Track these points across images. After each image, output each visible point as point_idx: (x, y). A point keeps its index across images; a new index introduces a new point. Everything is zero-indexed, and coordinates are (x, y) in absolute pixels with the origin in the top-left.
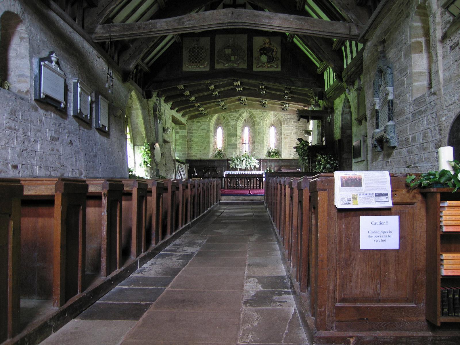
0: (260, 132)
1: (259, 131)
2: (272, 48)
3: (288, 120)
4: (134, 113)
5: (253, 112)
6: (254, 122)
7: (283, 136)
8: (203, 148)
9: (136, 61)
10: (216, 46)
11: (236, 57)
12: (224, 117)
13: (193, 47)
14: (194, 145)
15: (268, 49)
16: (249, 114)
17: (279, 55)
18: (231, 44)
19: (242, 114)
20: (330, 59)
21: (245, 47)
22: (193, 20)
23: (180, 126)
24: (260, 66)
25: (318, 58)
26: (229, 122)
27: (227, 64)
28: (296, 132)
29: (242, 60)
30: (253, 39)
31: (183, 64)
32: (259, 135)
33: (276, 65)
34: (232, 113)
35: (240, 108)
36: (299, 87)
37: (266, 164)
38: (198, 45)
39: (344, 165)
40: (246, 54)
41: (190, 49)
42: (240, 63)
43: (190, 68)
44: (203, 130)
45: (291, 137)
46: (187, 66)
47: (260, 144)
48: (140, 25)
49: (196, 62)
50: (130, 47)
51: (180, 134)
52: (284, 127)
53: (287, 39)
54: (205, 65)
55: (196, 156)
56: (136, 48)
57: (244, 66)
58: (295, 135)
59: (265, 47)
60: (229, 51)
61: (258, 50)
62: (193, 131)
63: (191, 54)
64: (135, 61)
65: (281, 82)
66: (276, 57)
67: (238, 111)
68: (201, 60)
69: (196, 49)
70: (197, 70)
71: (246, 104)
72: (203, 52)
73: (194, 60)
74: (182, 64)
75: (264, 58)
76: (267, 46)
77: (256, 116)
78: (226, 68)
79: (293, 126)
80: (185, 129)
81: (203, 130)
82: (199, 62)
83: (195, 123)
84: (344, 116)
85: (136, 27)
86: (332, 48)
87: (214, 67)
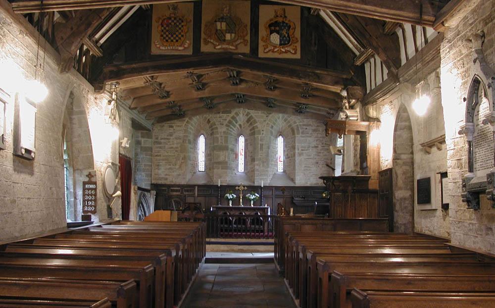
0: (263, 145)
1: (261, 143)
2: (287, 24)
4: (74, 118)
6: (253, 128)
11: (233, 35)
13: (168, 18)
15: (281, 24)
16: (246, 117)
17: (298, 34)
19: (235, 116)
21: (247, 20)
23: (142, 133)
24: (269, 51)
25: (358, 42)
26: (217, 128)
27: (219, 45)
28: (316, 145)
29: (242, 41)
32: (261, 148)
33: (293, 49)
34: (221, 115)
35: (234, 108)
36: (327, 84)
37: (271, 192)
38: (175, 14)
41: (163, 21)
43: (162, 50)
46: (158, 46)
47: (263, 162)
49: (172, 41)
52: (298, 137)
54: (186, 46)
55: (166, 179)
58: (315, 149)
59: (276, 22)
61: (267, 26)
62: (162, 141)
63: (165, 28)
67: (230, 113)
69: (173, 21)
72: (182, 26)
73: (170, 38)
75: (275, 38)
76: (280, 20)
79: (310, 137)
80: (149, 137)
81: (176, 138)
83: (165, 128)
84: (398, 133)
86: (384, 30)
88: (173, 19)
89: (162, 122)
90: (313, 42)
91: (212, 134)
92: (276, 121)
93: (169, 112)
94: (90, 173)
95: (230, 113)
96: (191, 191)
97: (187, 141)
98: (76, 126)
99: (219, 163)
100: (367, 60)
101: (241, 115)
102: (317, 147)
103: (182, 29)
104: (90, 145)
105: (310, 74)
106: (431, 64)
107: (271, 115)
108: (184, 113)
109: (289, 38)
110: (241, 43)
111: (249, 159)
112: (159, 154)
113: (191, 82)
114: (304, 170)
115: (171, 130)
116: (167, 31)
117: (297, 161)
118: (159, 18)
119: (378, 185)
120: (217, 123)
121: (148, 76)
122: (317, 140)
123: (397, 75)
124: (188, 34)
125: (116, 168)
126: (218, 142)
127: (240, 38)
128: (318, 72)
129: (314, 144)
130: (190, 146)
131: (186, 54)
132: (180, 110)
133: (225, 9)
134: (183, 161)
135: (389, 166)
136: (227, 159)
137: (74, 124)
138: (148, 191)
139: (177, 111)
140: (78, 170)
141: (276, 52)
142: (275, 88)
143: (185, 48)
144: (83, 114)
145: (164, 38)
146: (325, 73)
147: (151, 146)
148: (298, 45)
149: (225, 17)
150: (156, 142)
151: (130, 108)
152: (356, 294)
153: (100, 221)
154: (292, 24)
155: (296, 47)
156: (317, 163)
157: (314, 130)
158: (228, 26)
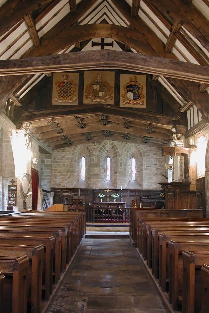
2: (137, 86)
5: (115, 144)
6: (116, 153)
7: (143, 167)
10: (85, 82)
11: (104, 93)
12: (88, 147)
17: (144, 92)
19: (104, 145)
21: (112, 83)
22: (70, 59)
24: (127, 103)
26: (93, 153)
27: (95, 99)
30: (120, 76)
31: (53, 97)
32: (121, 165)
34: (96, 144)
35: (103, 140)
38: (67, 80)
41: (59, 84)
43: (59, 102)
45: (150, 168)
46: (56, 100)
48: (16, 62)
49: (65, 97)
53: (152, 78)
54: (74, 100)
55: (60, 185)
58: (155, 166)
59: (131, 85)
62: (58, 160)
63: (61, 89)
65: (146, 118)
66: (142, 95)
69: (66, 84)
71: (109, 136)
72: (72, 87)
73: (64, 95)
76: (133, 83)
77: (118, 147)
80: (50, 158)
81: (67, 159)
82: (68, 97)
83: (59, 152)
85: (12, 64)
88: (66, 83)
90: (154, 97)
92: (130, 148)
93: (62, 142)
96: (76, 192)
99: (94, 175)
100: (188, 109)
101: (108, 144)
102: (157, 164)
103: (72, 89)
105: (152, 117)
111: (113, 172)
115: (64, 154)
116: (62, 90)
117: (144, 174)
118: (57, 82)
119: (196, 188)
121: (49, 119)
124: (75, 93)
126: (93, 161)
131: (74, 105)
132: (70, 141)
133: (99, 77)
134: (71, 173)
136: (99, 172)
140: (5, 177)
142: (130, 126)
143: (74, 101)
145: (60, 95)
147: (51, 164)
148: (145, 100)
149: (98, 82)
153: (19, 211)
154: (141, 86)
156: (157, 175)
157: (154, 154)
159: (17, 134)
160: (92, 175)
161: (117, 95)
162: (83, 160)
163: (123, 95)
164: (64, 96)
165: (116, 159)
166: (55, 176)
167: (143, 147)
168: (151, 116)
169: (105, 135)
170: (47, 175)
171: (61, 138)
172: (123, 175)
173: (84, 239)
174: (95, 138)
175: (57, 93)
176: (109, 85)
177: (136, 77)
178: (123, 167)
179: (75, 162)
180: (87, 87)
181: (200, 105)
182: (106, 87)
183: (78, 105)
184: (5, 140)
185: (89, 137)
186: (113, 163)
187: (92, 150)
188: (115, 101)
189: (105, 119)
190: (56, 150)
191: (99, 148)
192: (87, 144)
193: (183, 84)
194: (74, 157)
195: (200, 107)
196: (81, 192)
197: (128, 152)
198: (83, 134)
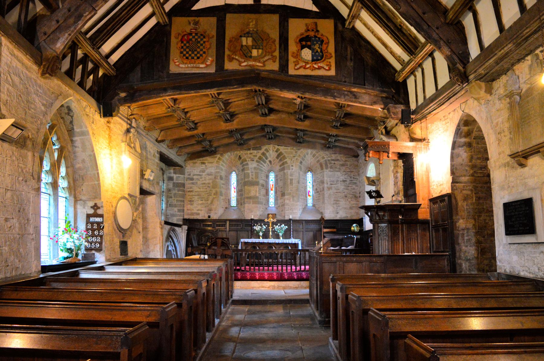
2: (319, 38)
3: (333, 162)
5: (281, 150)
7: (326, 185)
8: (209, 202)
9: (70, 35)
11: (260, 51)
14: (196, 197)
17: (331, 48)
18: (251, 29)
19: (265, 152)
20: (441, 39)
21: (275, 35)
23: (174, 169)
24: (301, 67)
26: (247, 164)
27: (244, 62)
29: (270, 57)
30: (288, 22)
32: (291, 183)
33: (327, 65)
34: (252, 151)
35: (264, 144)
36: (365, 103)
37: (301, 225)
38: (196, 30)
39: (460, 241)
40: (278, 46)
42: (266, 61)
43: (182, 68)
44: (208, 175)
46: (177, 64)
47: (293, 197)
49: (193, 58)
50: (59, 8)
51: (175, 181)
54: (208, 63)
55: (198, 214)
56: (69, 11)
57: (275, 66)
59: (308, 36)
60: (248, 42)
61: (298, 41)
62: (195, 177)
63: (185, 45)
64: (67, 35)
67: (260, 148)
68: (201, 55)
70: (193, 72)
71: (272, 138)
72: (204, 42)
73: (190, 55)
74: (169, 62)
75: (307, 54)
76: (312, 34)
77: (286, 155)
78: (243, 68)
80: (183, 173)
81: (208, 175)
82: (198, 58)
83: (197, 164)
84: (456, 151)
86: (446, 18)
87: (223, 67)
88: (194, 35)
89: (195, 159)
90: (349, 57)
91: (243, 170)
92: (305, 156)
93: (198, 148)
94: (96, 204)
95: (260, 149)
96: (222, 225)
97: (219, 177)
98: (79, 150)
99: (250, 198)
100: (412, 72)
101: (271, 150)
102: (345, 181)
103: (204, 45)
104: (96, 172)
105: (346, 93)
106: (531, 40)
107: (300, 151)
108: (215, 150)
109: (322, 53)
110: (268, 59)
111: (279, 194)
112: (191, 190)
113: (218, 111)
114: (334, 204)
115: (203, 166)
116: (187, 47)
117: (326, 195)
118: (179, 34)
119: (429, 214)
120: (247, 159)
121: (167, 98)
122: (346, 174)
123: (465, 72)
124: (210, 51)
125: (135, 201)
126: (249, 177)
127: (267, 54)
128: (355, 90)
129: (342, 178)
130: (222, 182)
131: (208, 72)
132: (211, 146)
133: (251, 24)
134: (214, 196)
135: (446, 189)
136: (258, 195)
137: (76, 147)
138: (179, 226)
139: (208, 146)
140: (81, 200)
141: (308, 68)
142: (306, 117)
143: (207, 66)
144: (86, 135)
145: (184, 55)
146: (363, 91)
147: (183, 182)
148: (333, 61)
149: (251, 32)
150: (189, 178)
151: (157, 140)
152: (372, 314)
153: (107, 260)
154: (325, 39)
155: (330, 62)
156: (346, 197)
157: (343, 165)
158: (254, 42)
159: (109, 125)
160: (248, 198)
161: (283, 54)
162: (234, 178)
163: (294, 53)
164: (190, 58)
165: (284, 173)
166: (190, 201)
167: (325, 155)
168: (344, 91)
169: (265, 136)
170: (177, 200)
171: (196, 141)
172: (295, 199)
173: (228, 310)
174: (251, 143)
175: (178, 52)
176: (269, 37)
177: (316, 24)
178: (294, 185)
179: (221, 178)
180: (230, 41)
181: (450, 48)
182: (265, 42)
183: (216, 71)
184: (78, 130)
185: (242, 139)
186: (279, 180)
187: (246, 161)
188: (280, 65)
189: (264, 103)
190: (192, 161)
191: (257, 157)
192: (238, 152)
193: (413, 9)
194: (219, 172)
195: (449, 54)
196: (230, 224)
197: (301, 163)
198: (231, 133)
